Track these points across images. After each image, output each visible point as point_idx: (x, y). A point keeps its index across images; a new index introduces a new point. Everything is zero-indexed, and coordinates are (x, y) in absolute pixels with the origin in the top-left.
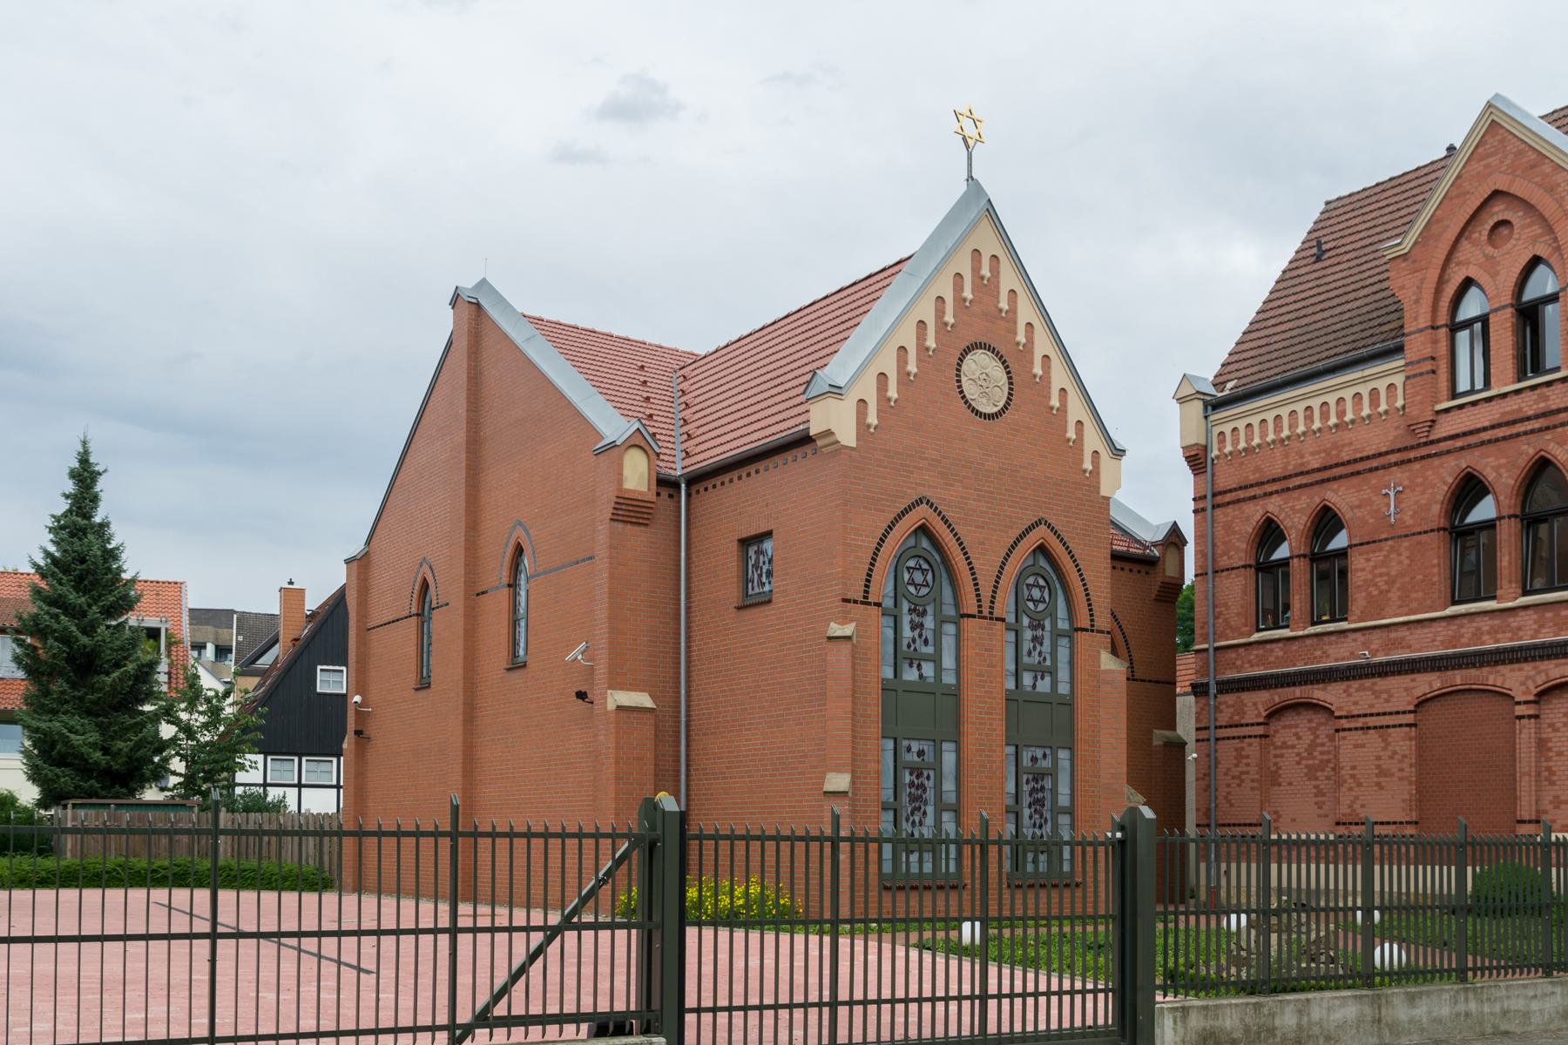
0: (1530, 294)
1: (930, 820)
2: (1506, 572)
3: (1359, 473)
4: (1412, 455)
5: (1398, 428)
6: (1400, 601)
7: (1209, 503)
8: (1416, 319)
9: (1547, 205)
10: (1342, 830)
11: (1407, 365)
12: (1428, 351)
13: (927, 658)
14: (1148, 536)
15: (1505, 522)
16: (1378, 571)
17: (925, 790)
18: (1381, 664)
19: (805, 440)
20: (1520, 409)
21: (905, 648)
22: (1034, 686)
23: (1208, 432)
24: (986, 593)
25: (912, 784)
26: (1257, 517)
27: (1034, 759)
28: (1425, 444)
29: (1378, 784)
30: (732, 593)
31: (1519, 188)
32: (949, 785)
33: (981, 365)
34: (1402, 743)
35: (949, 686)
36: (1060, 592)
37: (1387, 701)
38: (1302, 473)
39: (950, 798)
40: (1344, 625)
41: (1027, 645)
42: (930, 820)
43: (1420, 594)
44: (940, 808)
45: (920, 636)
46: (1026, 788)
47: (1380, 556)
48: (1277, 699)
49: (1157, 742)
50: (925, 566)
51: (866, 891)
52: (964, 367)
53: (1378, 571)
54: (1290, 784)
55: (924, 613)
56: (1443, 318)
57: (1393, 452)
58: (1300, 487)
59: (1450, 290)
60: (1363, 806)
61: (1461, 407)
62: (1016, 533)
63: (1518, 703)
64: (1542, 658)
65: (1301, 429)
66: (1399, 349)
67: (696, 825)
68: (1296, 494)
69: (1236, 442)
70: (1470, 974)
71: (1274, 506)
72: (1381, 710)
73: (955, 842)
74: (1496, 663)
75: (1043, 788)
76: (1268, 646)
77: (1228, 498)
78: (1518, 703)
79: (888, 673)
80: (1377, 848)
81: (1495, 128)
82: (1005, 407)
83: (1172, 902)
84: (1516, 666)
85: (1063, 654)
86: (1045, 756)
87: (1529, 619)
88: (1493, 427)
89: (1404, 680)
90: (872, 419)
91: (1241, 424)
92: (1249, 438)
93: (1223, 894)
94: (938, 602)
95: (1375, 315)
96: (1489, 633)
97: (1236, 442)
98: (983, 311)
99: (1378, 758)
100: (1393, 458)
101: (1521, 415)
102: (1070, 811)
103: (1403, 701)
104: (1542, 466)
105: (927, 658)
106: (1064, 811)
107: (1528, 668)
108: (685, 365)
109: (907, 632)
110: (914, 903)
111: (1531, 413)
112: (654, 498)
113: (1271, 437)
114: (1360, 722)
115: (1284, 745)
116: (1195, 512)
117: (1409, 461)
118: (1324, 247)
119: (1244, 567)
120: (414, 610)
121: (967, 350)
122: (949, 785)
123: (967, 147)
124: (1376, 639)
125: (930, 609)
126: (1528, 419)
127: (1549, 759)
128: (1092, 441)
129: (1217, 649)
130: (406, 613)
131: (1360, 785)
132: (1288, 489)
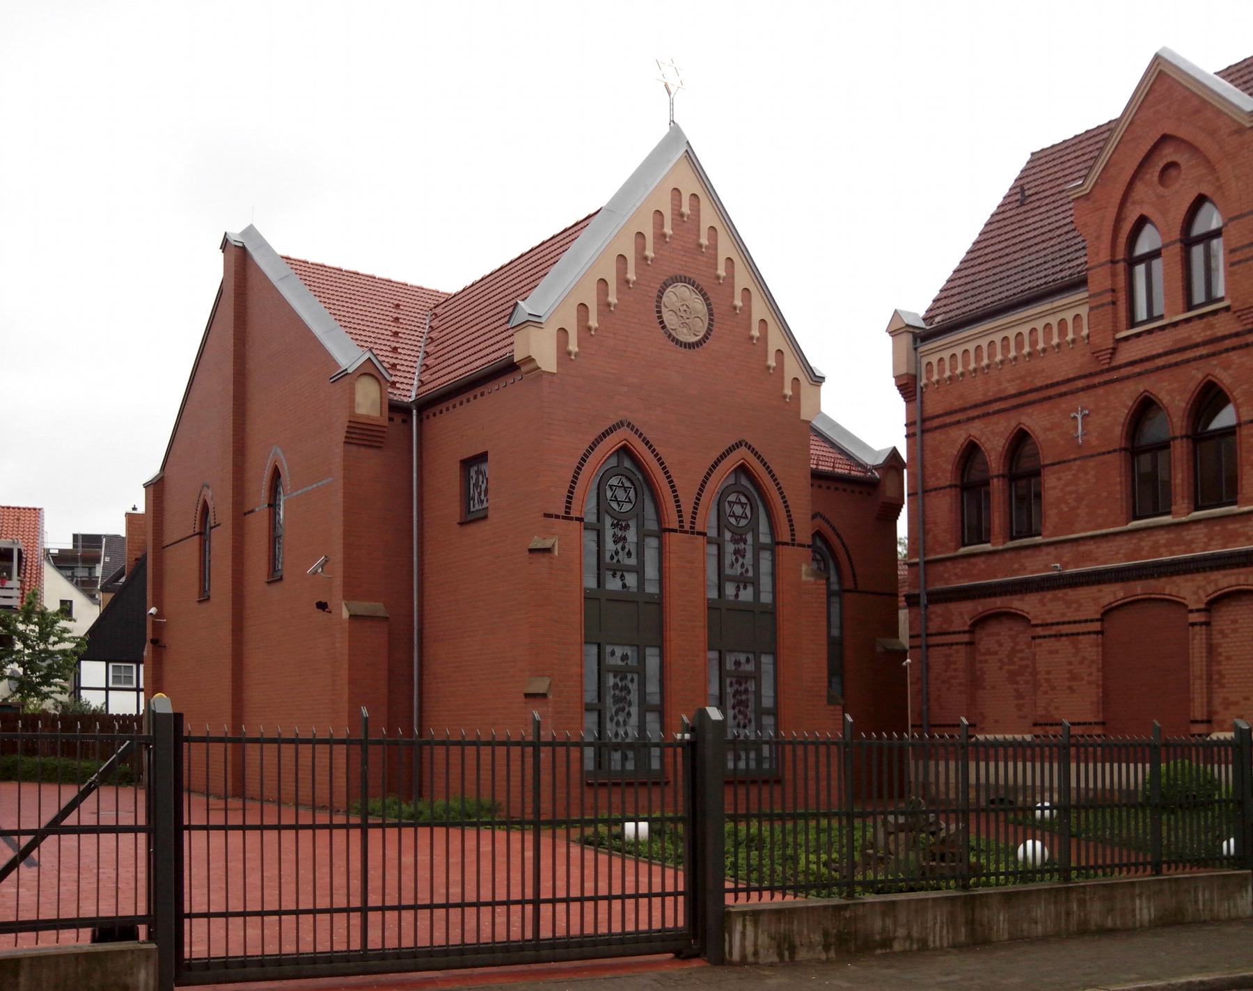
0: (1198, 229)
1: (634, 720)
2: (1179, 489)
3: (1050, 398)
4: (1096, 380)
5: (1083, 355)
6: (1085, 513)
7: (918, 427)
8: (1097, 254)
10: (1038, 731)
11: (1090, 297)
12: (1108, 284)
13: (630, 569)
14: (870, 461)
15: (1178, 442)
16: (1068, 489)
17: (629, 692)
18: (1072, 576)
19: (509, 368)
20: (1190, 337)
21: (608, 559)
22: (737, 596)
23: (917, 363)
24: (687, 508)
25: (615, 686)
26: (962, 440)
27: (737, 663)
28: (1108, 370)
29: (1070, 688)
30: (455, 510)
31: (1182, 133)
32: (653, 687)
33: (680, 295)
34: (1090, 649)
35: (653, 595)
36: (761, 509)
37: (1077, 610)
38: (1001, 399)
39: (654, 699)
41: (729, 558)
43: (1105, 511)
44: (644, 708)
45: (623, 548)
47: (1068, 476)
48: (980, 609)
49: (879, 649)
50: (627, 484)
51: (829, 785)
52: (665, 299)
53: (1068, 489)
54: (993, 688)
55: (627, 527)
57: (1079, 378)
58: (998, 412)
59: (1127, 227)
60: (1057, 708)
61: (1138, 335)
62: (715, 455)
63: (1191, 611)
64: (1212, 569)
65: (999, 358)
67: (188, 727)
68: (994, 419)
69: (941, 371)
70: (1165, 866)
71: (976, 430)
72: (1072, 619)
74: (1172, 574)
75: (746, 691)
76: (973, 560)
77: (936, 423)
78: (1191, 611)
79: (591, 583)
80: (1073, 750)
82: (706, 337)
84: (1189, 576)
85: (765, 566)
86: (748, 660)
87: (1199, 532)
88: (1166, 354)
89: (1092, 591)
90: (573, 347)
95: (1065, 252)
96: (1165, 546)
97: (941, 371)
99: (1070, 663)
100: (1080, 383)
101: (1192, 342)
102: (774, 712)
103: (1093, 611)
105: (630, 569)
106: (768, 712)
107: (1200, 578)
109: (610, 546)
111: (1199, 340)
115: (988, 652)
116: (907, 436)
117: (1094, 386)
118: (1027, 193)
119: (950, 486)
120: (197, 530)
121: (665, 286)
122: (653, 687)
123: (669, 93)
124: (1067, 552)
125: (632, 524)
126: (1197, 345)
127: (1219, 663)
128: (792, 369)
129: (926, 563)
130: (191, 532)
131: (1054, 688)
132: (988, 414)
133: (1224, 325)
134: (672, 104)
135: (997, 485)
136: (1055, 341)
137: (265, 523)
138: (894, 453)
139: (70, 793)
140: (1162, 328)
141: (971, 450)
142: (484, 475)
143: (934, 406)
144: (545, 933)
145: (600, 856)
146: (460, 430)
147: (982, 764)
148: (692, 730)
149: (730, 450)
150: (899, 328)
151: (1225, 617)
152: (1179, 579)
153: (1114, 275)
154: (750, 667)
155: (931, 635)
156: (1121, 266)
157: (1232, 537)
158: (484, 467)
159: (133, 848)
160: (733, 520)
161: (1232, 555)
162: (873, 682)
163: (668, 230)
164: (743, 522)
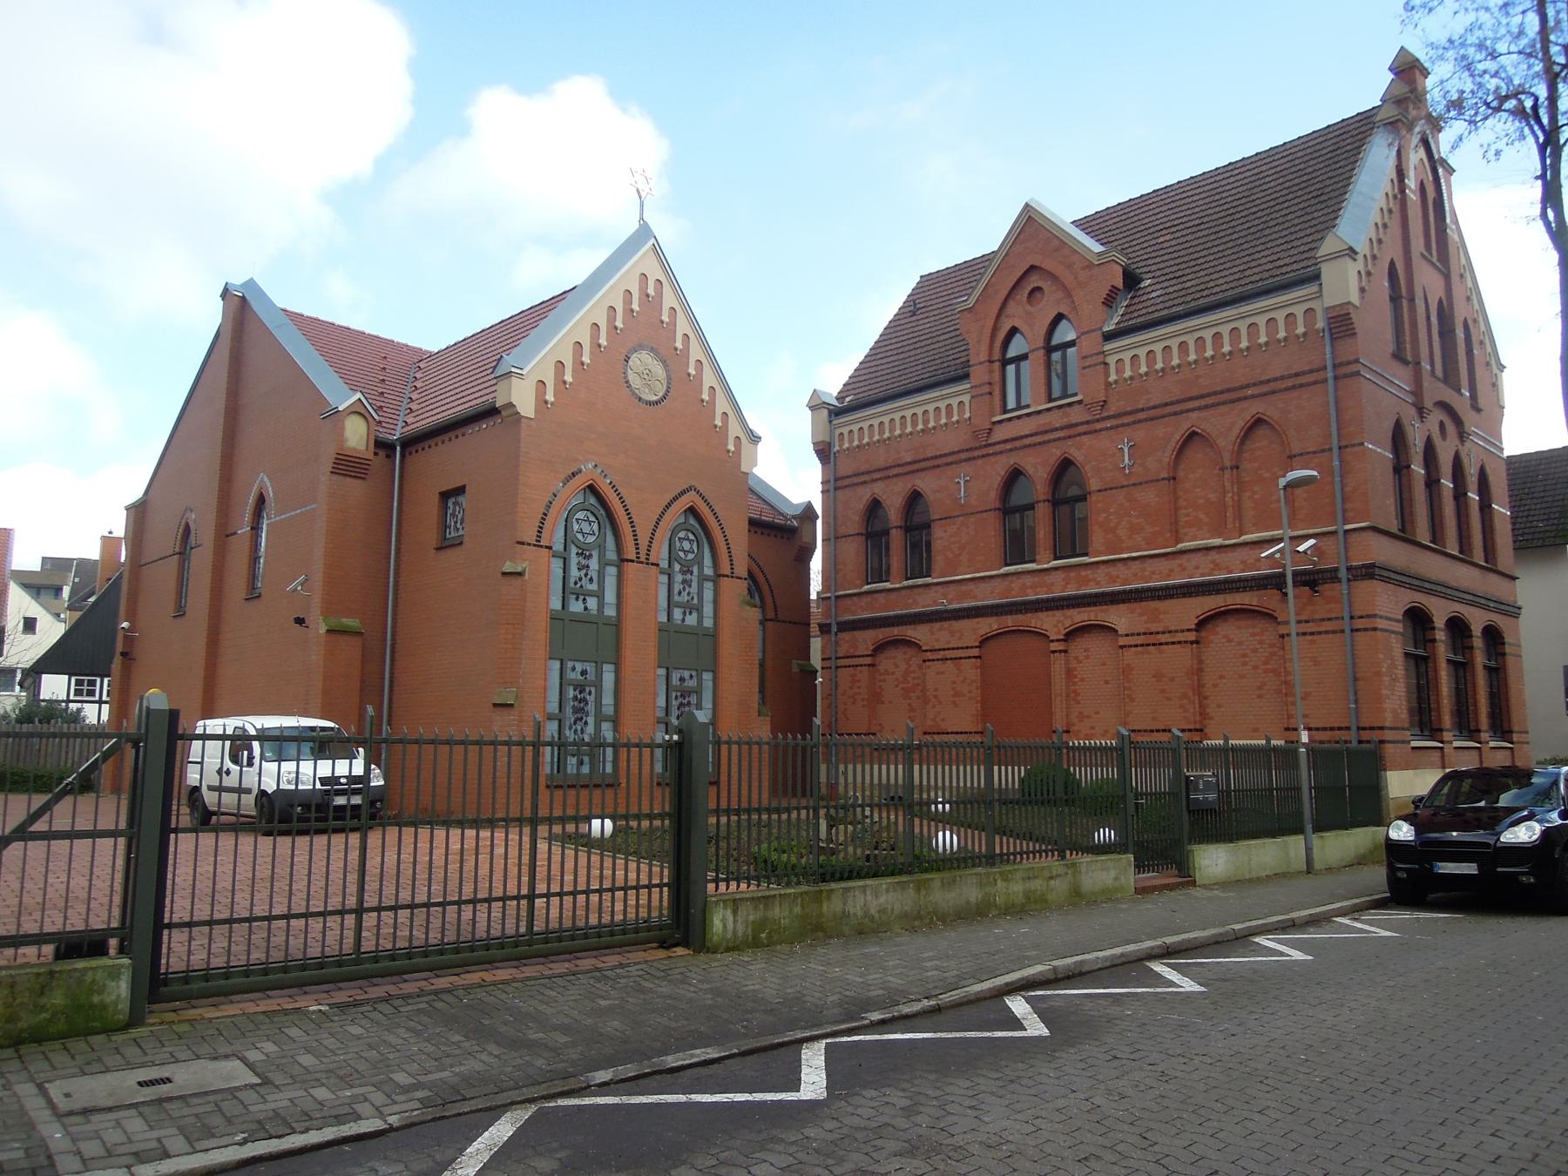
4: (976, 453)
7: (833, 485)
9: (1067, 278)
12: (986, 379)
14: (790, 512)
18: (955, 610)
19: (491, 412)
23: (832, 433)
24: (643, 543)
25: (575, 698)
30: (432, 538)
31: (1048, 265)
32: (608, 699)
34: (970, 670)
39: (608, 709)
40: (929, 580)
41: (677, 587)
42: (590, 729)
46: (675, 703)
55: (590, 556)
56: (996, 356)
61: (1010, 419)
64: (1068, 607)
65: (898, 432)
66: (966, 376)
69: (851, 441)
71: (879, 489)
73: (613, 745)
77: (847, 482)
79: (556, 604)
81: (1030, 224)
83: (794, 795)
91: (855, 428)
92: (861, 439)
93: (841, 789)
94: (601, 548)
97: (851, 441)
98: (646, 324)
100: (963, 456)
104: (1066, 464)
107: (1058, 614)
108: (418, 359)
109: (574, 572)
110: (571, 800)
112: (371, 456)
113: (876, 437)
114: (941, 655)
115: (887, 672)
125: (595, 554)
128: (734, 430)
129: (1346, 532)
133: (1077, 415)
134: (642, 206)
135: (896, 536)
136: (943, 421)
137: (246, 545)
138: (809, 507)
139: (45, 798)
140: (1028, 415)
141: (875, 506)
142: (460, 505)
143: (846, 467)
144: (539, 926)
145: (593, 858)
146: (444, 464)
147: (884, 767)
148: (680, 732)
149: (683, 493)
150: (816, 405)
151: (1079, 646)
152: (1113, 609)
153: (991, 371)
154: (692, 683)
155: (1364, 729)
156: (997, 365)
157: (1085, 582)
158: (460, 499)
159: (109, 856)
160: (682, 554)
161: (1085, 596)
162: (789, 692)
163: (635, 307)
164: (691, 556)
